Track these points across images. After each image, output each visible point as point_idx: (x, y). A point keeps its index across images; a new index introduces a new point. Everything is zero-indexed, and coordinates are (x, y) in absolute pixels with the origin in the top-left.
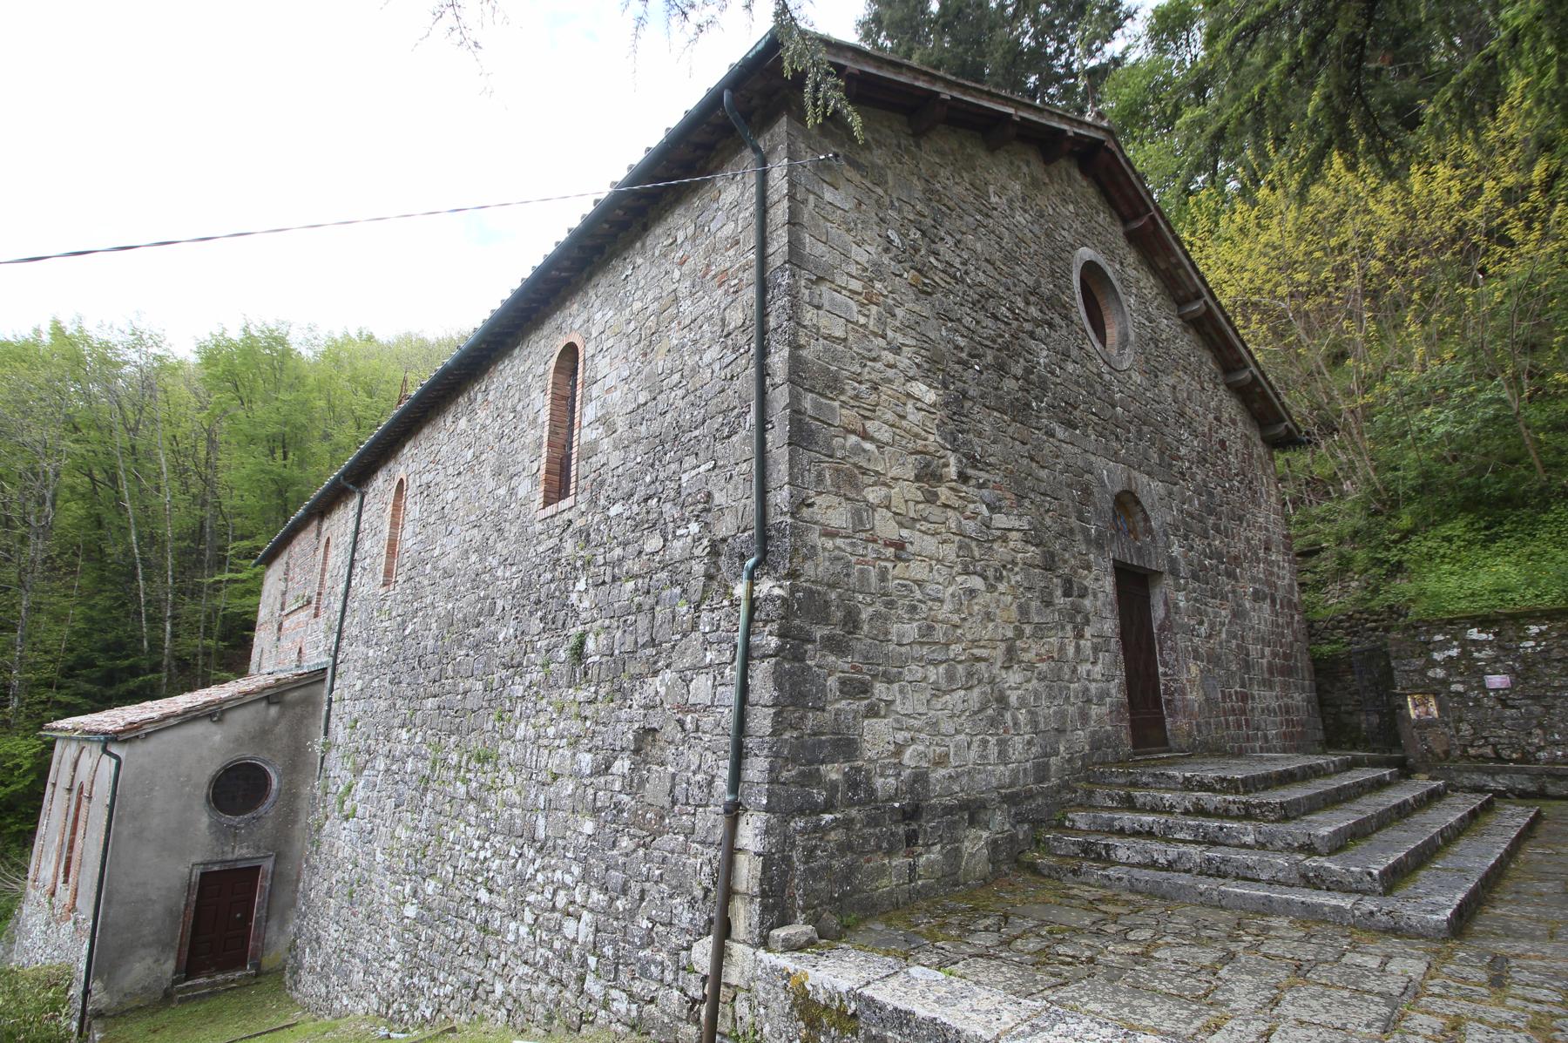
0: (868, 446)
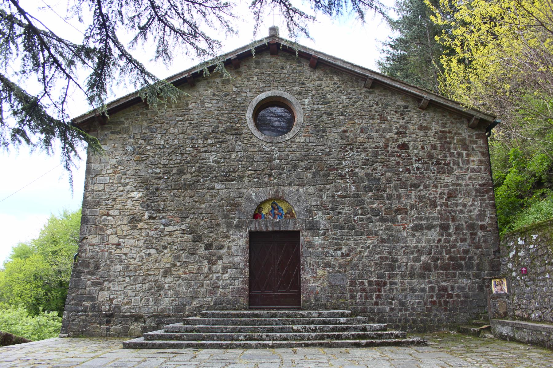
0: (109, 218)
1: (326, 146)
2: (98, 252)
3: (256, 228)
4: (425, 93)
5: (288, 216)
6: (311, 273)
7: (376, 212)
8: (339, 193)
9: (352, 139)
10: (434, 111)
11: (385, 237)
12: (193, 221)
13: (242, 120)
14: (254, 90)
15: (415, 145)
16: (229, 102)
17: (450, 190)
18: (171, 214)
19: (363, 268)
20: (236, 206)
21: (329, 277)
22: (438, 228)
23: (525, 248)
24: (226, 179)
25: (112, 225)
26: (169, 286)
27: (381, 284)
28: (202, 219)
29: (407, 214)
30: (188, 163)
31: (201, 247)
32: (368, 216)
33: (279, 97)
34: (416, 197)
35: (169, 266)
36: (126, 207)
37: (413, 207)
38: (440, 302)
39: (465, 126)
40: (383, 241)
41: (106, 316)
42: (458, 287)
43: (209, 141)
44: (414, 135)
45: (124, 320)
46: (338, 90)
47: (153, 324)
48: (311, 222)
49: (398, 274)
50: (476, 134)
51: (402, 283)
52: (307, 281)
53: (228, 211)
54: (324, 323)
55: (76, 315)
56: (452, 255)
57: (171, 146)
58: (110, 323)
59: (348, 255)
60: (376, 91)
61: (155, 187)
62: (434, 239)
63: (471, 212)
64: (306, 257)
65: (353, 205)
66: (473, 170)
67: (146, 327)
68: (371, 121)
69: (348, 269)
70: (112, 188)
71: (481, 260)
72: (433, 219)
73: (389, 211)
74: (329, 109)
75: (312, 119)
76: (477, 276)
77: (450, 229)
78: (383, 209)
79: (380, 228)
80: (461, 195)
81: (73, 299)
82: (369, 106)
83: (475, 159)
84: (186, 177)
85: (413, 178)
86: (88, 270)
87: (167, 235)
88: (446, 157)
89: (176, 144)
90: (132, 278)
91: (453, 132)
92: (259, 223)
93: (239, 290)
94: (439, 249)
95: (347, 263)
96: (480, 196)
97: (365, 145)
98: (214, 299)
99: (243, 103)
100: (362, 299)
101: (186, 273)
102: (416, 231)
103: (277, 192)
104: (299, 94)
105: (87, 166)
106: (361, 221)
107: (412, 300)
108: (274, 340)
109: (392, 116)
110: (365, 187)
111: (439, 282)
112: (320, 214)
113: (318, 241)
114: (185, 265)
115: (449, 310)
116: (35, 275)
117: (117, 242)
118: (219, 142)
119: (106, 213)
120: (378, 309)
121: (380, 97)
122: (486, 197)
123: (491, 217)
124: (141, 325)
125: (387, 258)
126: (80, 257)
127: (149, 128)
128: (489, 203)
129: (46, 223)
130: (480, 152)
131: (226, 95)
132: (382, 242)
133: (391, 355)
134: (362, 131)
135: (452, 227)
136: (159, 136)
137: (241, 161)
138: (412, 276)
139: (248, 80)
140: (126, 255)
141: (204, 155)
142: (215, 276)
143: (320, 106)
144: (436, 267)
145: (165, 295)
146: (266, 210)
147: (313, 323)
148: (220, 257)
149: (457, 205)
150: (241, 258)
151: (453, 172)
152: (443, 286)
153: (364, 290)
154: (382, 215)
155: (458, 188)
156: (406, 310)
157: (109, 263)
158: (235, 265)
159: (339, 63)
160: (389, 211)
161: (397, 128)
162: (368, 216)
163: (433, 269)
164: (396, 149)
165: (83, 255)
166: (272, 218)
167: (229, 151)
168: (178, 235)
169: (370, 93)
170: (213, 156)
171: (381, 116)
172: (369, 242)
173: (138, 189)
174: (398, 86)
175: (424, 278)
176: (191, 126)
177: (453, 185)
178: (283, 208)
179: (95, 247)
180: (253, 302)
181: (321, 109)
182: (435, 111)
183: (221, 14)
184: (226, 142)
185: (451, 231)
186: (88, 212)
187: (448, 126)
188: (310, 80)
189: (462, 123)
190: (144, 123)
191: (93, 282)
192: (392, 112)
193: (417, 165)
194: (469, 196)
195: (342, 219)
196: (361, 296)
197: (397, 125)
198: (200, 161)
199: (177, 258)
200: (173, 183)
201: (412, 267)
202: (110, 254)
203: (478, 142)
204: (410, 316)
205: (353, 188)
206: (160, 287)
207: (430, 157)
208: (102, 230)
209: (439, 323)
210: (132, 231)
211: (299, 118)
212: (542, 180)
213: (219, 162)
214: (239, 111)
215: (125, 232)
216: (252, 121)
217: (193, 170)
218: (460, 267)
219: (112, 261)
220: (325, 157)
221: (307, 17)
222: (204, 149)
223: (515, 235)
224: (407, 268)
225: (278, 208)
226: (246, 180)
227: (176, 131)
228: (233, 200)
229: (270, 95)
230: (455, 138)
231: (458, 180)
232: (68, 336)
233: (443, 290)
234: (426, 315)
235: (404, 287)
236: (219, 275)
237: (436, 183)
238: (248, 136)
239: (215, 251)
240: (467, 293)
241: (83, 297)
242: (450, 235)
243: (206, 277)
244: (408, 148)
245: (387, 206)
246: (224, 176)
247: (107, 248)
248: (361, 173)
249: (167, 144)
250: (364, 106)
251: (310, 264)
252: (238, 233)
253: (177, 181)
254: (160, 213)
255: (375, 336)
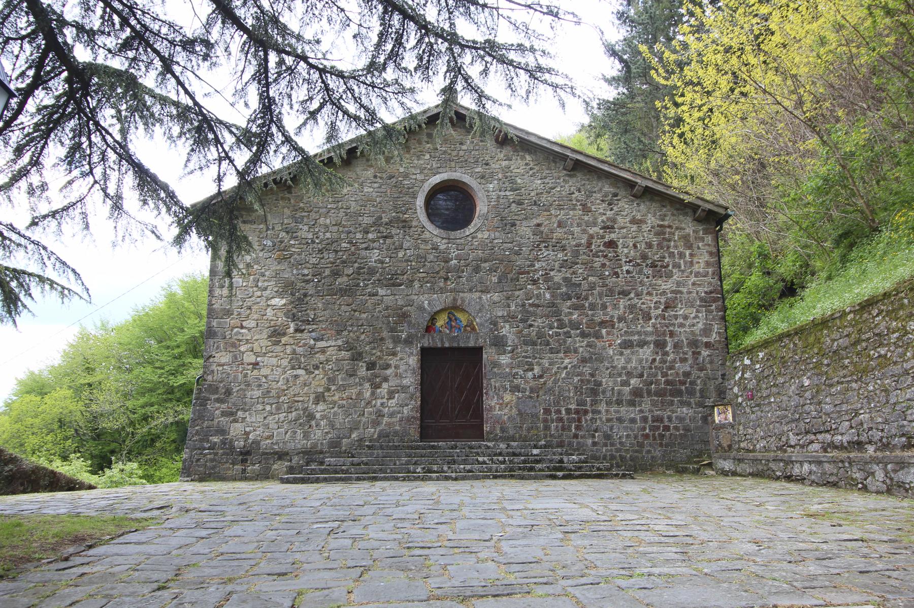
0: (243, 331)
1: (515, 243)
2: (229, 374)
3: (429, 343)
4: (639, 177)
5: (468, 329)
6: (496, 398)
7: (575, 325)
8: (530, 301)
9: (547, 235)
10: (650, 200)
11: (587, 355)
12: (351, 334)
13: (411, 209)
14: (426, 171)
15: (626, 242)
16: (395, 186)
17: (667, 298)
18: (324, 326)
19: (559, 392)
20: (404, 316)
21: (517, 404)
22: (652, 345)
23: (751, 369)
24: (392, 283)
25: (247, 340)
26: (321, 415)
27: (582, 412)
28: (363, 333)
29: (613, 328)
30: (344, 262)
31: (362, 366)
32: (565, 330)
33: (457, 181)
34: (625, 307)
35: (321, 390)
36: (264, 317)
37: (620, 319)
38: (654, 435)
39: (689, 219)
40: (584, 361)
41: (241, 453)
42: (677, 417)
43: (370, 236)
44: (625, 230)
45: (264, 459)
46: (531, 172)
47: (301, 462)
48: (496, 337)
49: (601, 400)
50: (703, 229)
51: (607, 411)
52: (491, 409)
53: (396, 323)
54: (514, 454)
55: (201, 454)
56: (670, 378)
57: (322, 241)
58: (246, 462)
59: (541, 377)
60: (578, 175)
61: (302, 292)
62: (647, 359)
63: (693, 325)
64: (490, 379)
65: (547, 316)
66: (697, 274)
67: (293, 467)
68: (571, 212)
69: (541, 393)
70: (247, 292)
71: (705, 384)
72: (646, 333)
73: (591, 323)
74: (519, 197)
75: (498, 210)
76: (701, 405)
77: (666, 347)
78: (584, 321)
79: (581, 344)
80: (682, 304)
81: (197, 433)
82: (570, 194)
83: (700, 261)
84: (342, 281)
85: (621, 284)
86: (216, 396)
87: (318, 352)
88: (664, 257)
89: (328, 239)
90: (274, 406)
91: (674, 227)
92: (433, 338)
93: (409, 419)
94: (654, 370)
95: (540, 386)
96: (705, 306)
97: (564, 242)
98: (377, 430)
99: (412, 188)
100: (558, 431)
101: (343, 399)
102: (625, 348)
103: (455, 299)
104: (483, 177)
105: (211, 265)
106: (557, 336)
107: (620, 433)
108: (456, 472)
109: (597, 207)
110: (562, 294)
111: (653, 411)
112: (507, 326)
113: (505, 359)
114: (342, 389)
115: (665, 445)
116: (60, 421)
117: (253, 361)
118: (382, 237)
119: (239, 325)
120: (578, 443)
121: (583, 182)
122: (714, 307)
123: (719, 333)
124: (286, 463)
125: (589, 381)
126: (205, 380)
127: (293, 217)
128: (717, 315)
129: (72, 339)
130: (707, 252)
131: (391, 177)
132: (582, 361)
133: (590, 484)
134: (560, 225)
135: (669, 345)
136: (306, 228)
137: (411, 261)
138: (619, 403)
139: (419, 158)
140: (266, 377)
141: (363, 253)
142: (379, 402)
143: (508, 193)
144: (649, 393)
145: (316, 426)
146: (441, 322)
147: (500, 454)
148: (386, 379)
149: (676, 317)
150: (411, 380)
151: (672, 276)
152: (657, 416)
153: (561, 420)
154: (582, 328)
155: (678, 296)
156: (612, 445)
157: (244, 387)
158: (404, 389)
159: (533, 139)
160: (591, 323)
161: (603, 221)
162: (565, 330)
163: (645, 395)
164: (602, 248)
165: (210, 378)
166: (448, 332)
167: (395, 249)
168: (333, 353)
169: (570, 176)
170: (375, 255)
171: (584, 206)
172: (567, 361)
173: (280, 295)
174: (606, 169)
175: (634, 405)
176: (347, 215)
177: (672, 292)
178: (462, 319)
179: (225, 367)
180: (425, 434)
181: (509, 197)
182: (652, 200)
183: (404, 100)
184: (392, 237)
185: (668, 349)
186: (214, 323)
187: (667, 218)
188: (496, 159)
189: (686, 214)
190: (286, 210)
191: (223, 412)
192: (598, 201)
193: (627, 268)
194: (692, 306)
195: (534, 333)
196: (557, 427)
197: (604, 218)
198: (358, 260)
199: (332, 380)
200: (326, 287)
201: (619, 393)
202: (246, 376)
203: (706, 239)
204: (617, 452)
205: (548, 296)
206: (311, 417)
207: (644, 257)
208: (234, 345)
209: (652, 461)
210: (274, 347)
211: (481, 207)
212: (794, 285)
213: (382, 262)
214: (407, 198)
215: (264, 348)
216: (424, 211)
217: (350, 271)
218: (679, 393)
219: (249, 385)
220: (514, 257)
221: (501, 104)
222: (364, 246)
223: (741, 354)
224: (613, 394)
225: (456, 319)
226: (417, 285)
227: (328, 221)
228: (401, 309)
229: (446, 178)
230: (677, 233)
231: (678, 286)
232: (192, 480)
233: (657, 421)
234: (637, 451)
235: (609, 416)
236: (385, 400)
237: (650, 289)
238: (419, 229)
239: (379, 371)
240: (688, 425)
241: (210, 431)
242: (666, 354)
243: (367, 404)
244: (617, 246)
245: (588, 318)
246: (390, 279)
247: (241, 369)
248: (558, 277)
249: (317, 238)
250: (563, 193)
251: (495, 387)
252: (407, 349)
253: (331, 285)
254: (309, 324)
255: (573, 468)
